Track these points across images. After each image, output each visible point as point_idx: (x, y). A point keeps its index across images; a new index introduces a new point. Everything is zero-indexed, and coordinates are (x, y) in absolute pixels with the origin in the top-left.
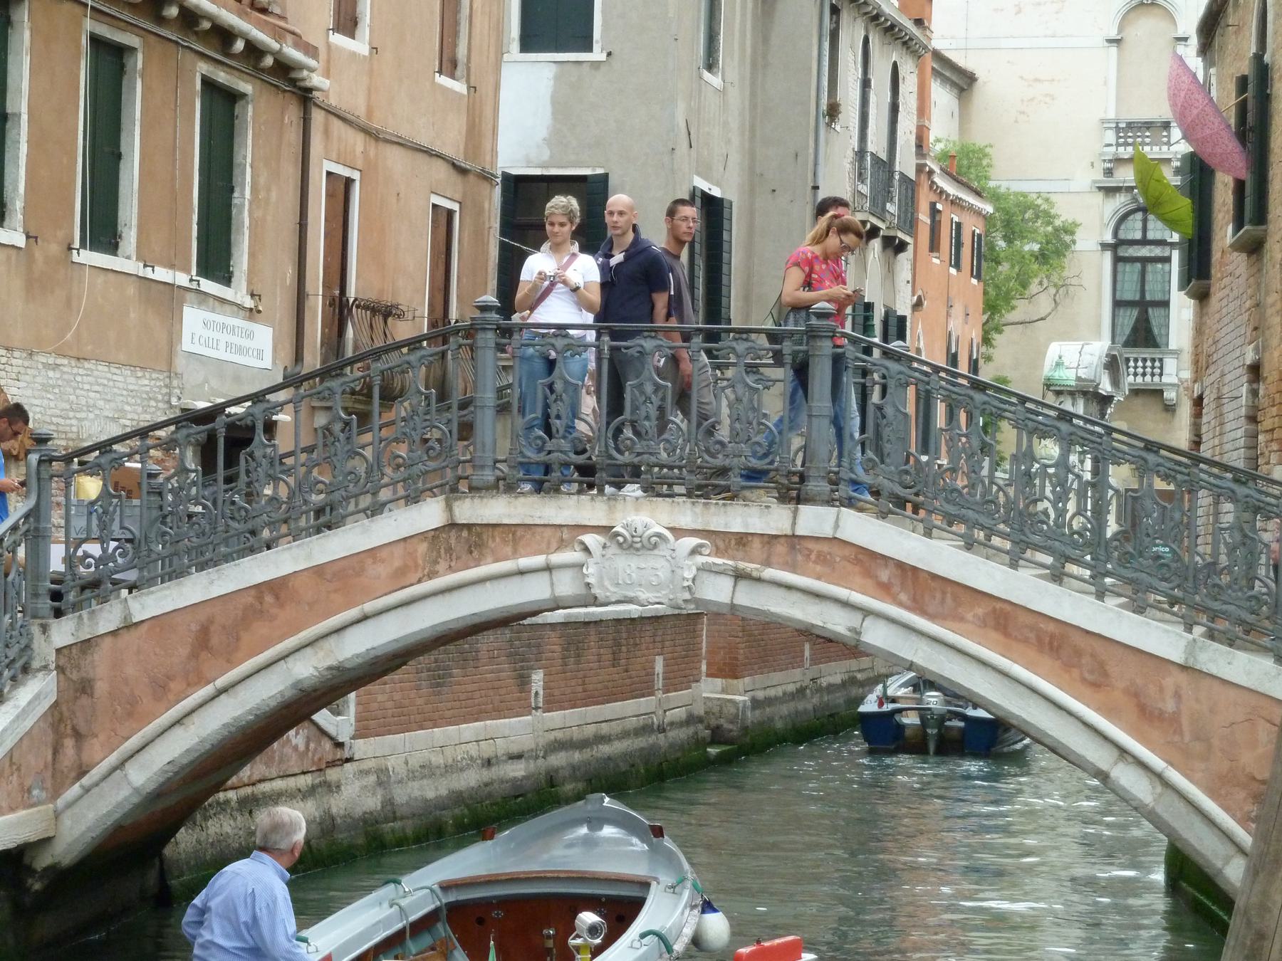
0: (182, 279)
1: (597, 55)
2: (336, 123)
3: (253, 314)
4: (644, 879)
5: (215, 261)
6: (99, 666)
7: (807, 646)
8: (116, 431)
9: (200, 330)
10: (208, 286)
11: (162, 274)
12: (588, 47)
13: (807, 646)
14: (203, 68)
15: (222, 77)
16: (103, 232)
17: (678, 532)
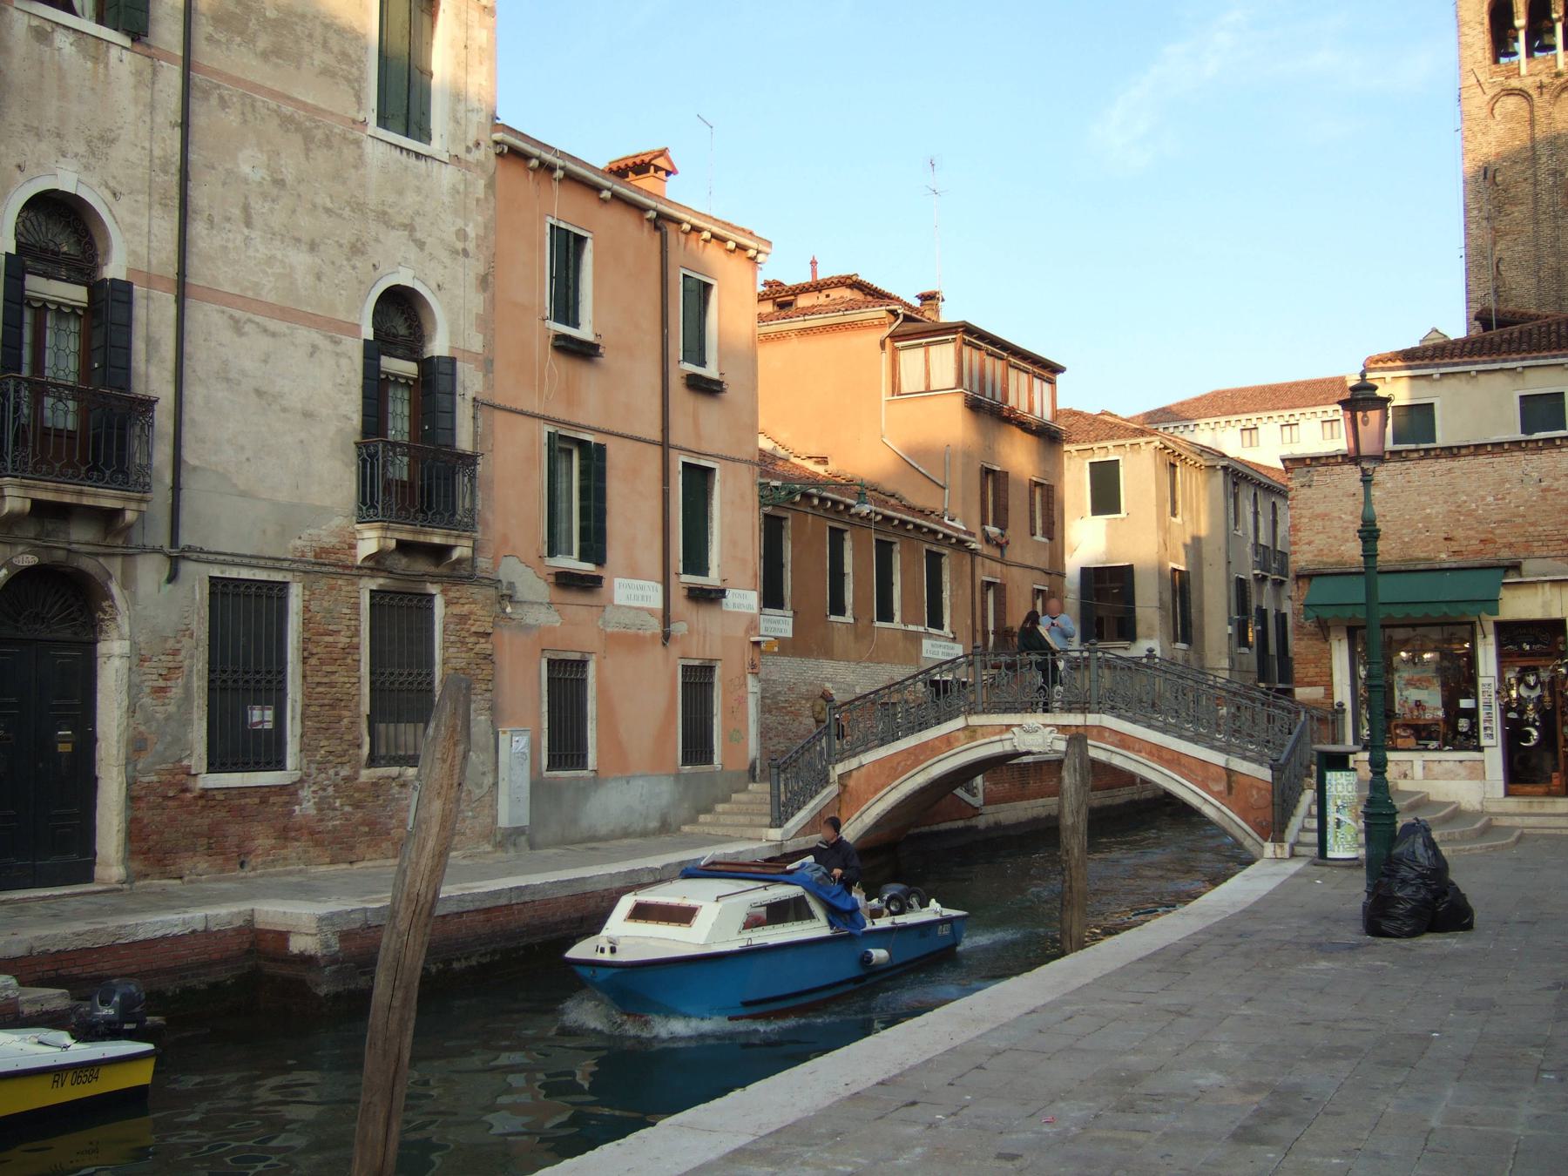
0: (921, 629)
1: (1123, 514)
2: (987, 561)
3: (954, 640)
4: (1453, 613)
5: (936, 621)
6: (851, 783)
7: (865, 1162)
8: (880, 686)
9: (782, 626)
10: (931, 630)
11: (911, 628)
12: (1119, 512)
13: (865, 1162)
14: (927, 546)
15: (935, 549)
16: (885, 614)
17: (1046, 726)
